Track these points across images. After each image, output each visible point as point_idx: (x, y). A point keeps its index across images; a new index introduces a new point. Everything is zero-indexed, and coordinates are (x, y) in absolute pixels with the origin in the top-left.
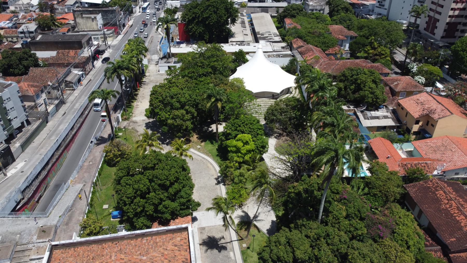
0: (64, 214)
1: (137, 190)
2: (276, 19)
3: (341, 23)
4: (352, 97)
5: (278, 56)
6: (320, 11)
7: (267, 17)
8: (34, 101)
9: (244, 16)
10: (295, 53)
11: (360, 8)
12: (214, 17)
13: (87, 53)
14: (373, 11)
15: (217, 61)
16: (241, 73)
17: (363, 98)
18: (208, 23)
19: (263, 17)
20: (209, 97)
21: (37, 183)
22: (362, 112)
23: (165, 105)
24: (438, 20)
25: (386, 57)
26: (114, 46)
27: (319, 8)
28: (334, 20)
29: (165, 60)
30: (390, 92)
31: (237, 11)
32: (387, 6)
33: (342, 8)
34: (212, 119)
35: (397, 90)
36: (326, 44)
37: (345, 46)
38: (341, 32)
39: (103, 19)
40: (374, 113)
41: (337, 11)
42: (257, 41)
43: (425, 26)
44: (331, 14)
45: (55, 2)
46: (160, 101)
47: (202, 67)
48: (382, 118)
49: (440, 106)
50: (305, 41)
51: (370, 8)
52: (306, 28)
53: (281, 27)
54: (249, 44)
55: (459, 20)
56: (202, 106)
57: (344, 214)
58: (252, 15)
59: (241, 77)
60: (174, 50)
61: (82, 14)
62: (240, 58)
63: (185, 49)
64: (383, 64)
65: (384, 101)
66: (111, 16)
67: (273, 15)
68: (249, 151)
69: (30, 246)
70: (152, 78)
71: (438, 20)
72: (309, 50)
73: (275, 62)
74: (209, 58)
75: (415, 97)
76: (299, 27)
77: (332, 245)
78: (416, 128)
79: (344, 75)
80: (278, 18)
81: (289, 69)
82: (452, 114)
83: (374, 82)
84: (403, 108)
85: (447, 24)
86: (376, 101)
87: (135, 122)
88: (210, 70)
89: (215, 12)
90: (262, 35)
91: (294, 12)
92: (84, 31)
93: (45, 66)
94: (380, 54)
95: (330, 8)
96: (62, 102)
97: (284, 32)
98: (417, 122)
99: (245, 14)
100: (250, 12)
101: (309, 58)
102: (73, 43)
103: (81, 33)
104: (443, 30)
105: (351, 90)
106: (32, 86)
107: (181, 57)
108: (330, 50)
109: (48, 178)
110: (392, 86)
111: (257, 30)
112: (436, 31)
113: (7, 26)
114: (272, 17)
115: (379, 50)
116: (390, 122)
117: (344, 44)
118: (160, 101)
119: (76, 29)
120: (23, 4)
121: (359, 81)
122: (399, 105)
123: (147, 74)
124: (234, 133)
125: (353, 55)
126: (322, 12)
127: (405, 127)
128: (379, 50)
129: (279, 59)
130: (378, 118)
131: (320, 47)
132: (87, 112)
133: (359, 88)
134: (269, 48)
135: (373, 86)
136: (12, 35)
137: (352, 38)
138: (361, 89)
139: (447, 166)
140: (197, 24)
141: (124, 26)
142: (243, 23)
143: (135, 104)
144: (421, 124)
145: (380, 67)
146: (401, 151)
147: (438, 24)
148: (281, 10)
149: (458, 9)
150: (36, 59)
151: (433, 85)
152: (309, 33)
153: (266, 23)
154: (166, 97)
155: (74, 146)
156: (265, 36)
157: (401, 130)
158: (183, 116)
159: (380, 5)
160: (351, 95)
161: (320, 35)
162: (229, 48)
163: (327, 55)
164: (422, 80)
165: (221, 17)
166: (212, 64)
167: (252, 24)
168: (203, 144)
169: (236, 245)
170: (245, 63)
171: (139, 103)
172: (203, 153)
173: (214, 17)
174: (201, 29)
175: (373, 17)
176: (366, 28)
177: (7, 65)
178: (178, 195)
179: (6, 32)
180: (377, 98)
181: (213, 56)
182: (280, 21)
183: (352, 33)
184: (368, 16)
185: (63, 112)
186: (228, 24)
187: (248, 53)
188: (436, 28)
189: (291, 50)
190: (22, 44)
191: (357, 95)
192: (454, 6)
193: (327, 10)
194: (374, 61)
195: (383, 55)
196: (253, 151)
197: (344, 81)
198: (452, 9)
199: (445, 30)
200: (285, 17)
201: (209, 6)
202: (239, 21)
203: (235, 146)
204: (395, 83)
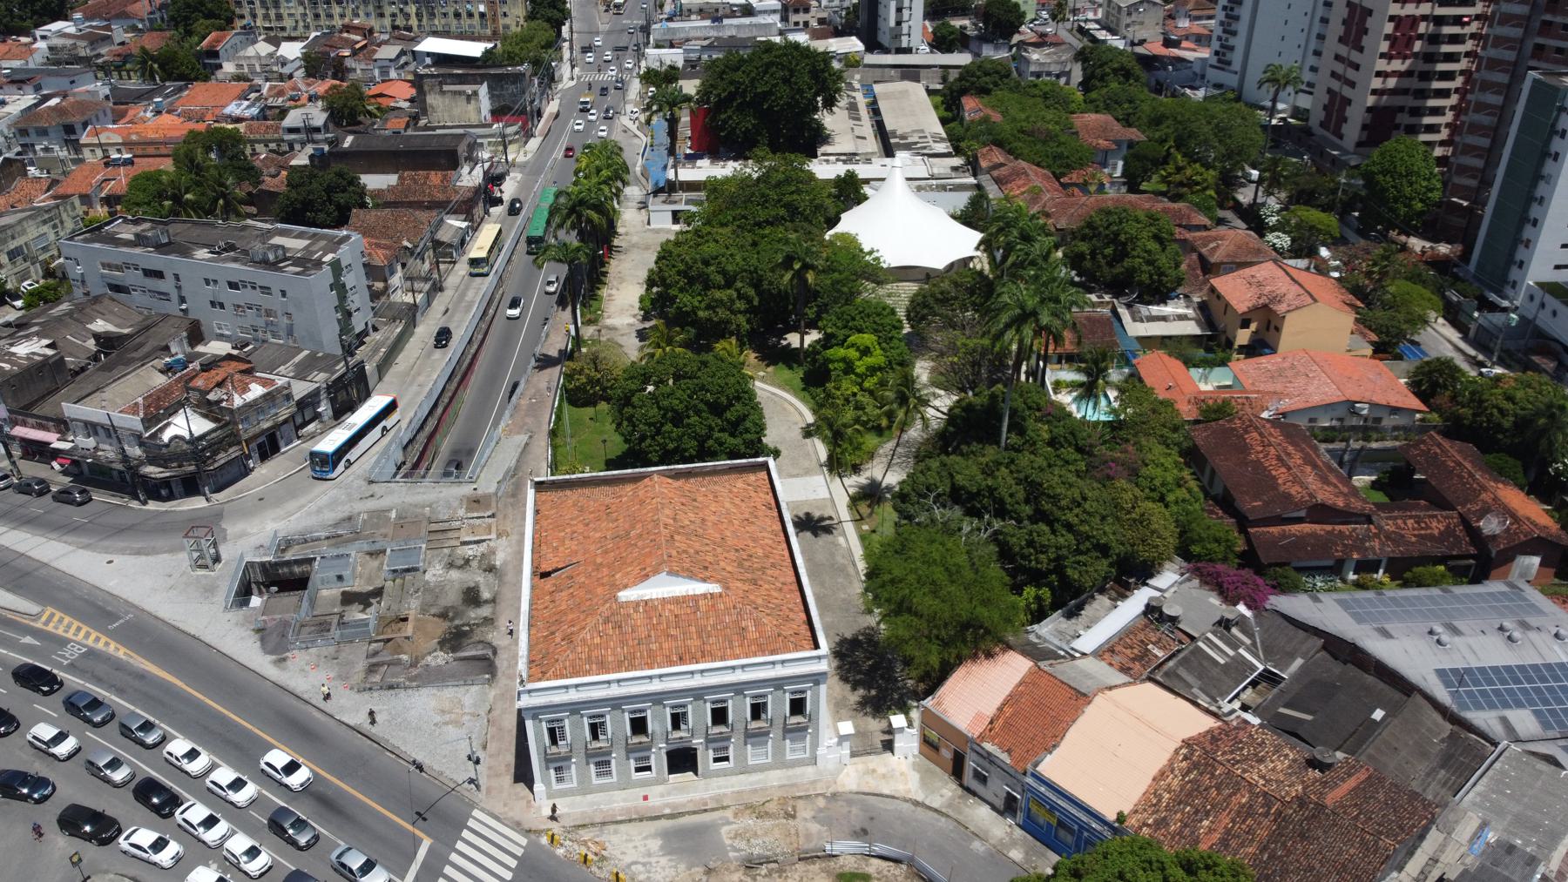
0: (504, 478)
1: (666, 410)
2: (939, 99)
3: (1108, 108)
4: (1107, 272)
5: (943, 188)
6: (1058, 76)
7: (916, 92)
8: (385, 281)
9: (854, 90)
10: (985, 180)
11: (1166, 69)
12: (784, 91)
13: (470, 177)
14: (1203, 77)
15: (798, 192)
16: (851, 223)
17: (1131, 272)
18: (762, 105)
19: (905, 93)
20: (788, 262)
21: (422, 437)
22: (1129, 306)
23: (691, 281)
24: (1349, 102)
25: (1205, 189)
26: (523, 166)
27: (1055, 69)
28: (1092, 101)
29: (662, 197)
30: (1198, 265)
31: (839, 76)
32: (1236, 66)
33: (1115, 71)
34: (786, 322)
35: (1212, 260)
36: (1063, 161)
37: (1114, 168)
38: (1103, 131)
39: (492, 97)
40: (1155, 310)
41: (1102, 79)
42: (889, 151)
43: (1322, 115)
44: (1086, 85)
45: (346, 53)
46: (679, 273)
47: (763, 204)
48: (1176, 318)
49: (1295, 289)
50: (1010, 152)
51: (1197, 69)
52: (1014, 120)
53: (953, 120)
54: (868, 161)
55: (1399, 101)
56: (771, 283)
57: (1046, 436)
58: (877, 88)
59: (853, 232)
60: (687, 174)
61: (441, 83)
62: (850, 192)
63: (704, 170)
64: (1196, 205)
65: (1179, 281)
66: (512, 88)
67: (932, 87)
68: (872, 370)
69: (456, 524)
70: (635, 239)
71: (1349, 102)
72: (1018, 173)
73: (934, 202)
74: (779, 184)
75: (1247, 272)
76: (996, 117)
77: (1019, 472)
78: (1243, 337)
79: (1090, 225)
80: (944, 95)
81: (967, 218)
82: (1315, 301)
83: (1157, 238)
84: (1219, 297)
85: (1369, 110)
86: (1160, 281)
87: (613, 329)
88: (782, 212)
89: (786, 81)
90: (903, 137)
91: (987, 79)
92: (444, 127)
93: (376, 206)
94: (1190, 184)
95: (1084, 69)
96: (437, 288)
97: (959, 130)
98: (1245, 324)
99: (857, 85)
100: (870, 81)
101: (1017, 189)
102: (437, 153)
103: (439, 132)
104: (1359, 127)
105: (1105, 257)
106: (378, 246)
107: (711, 186)
108: (1074, 176)
109: (438, 436)
110: (1204, 251)
111: (889, 127)
112: (1345, 129)
113: (247, 114)
114: (930, 92)
115: (1189, 172)
116: (1191, 328)
117: (1111, 162)
118: (679, 273)
119: (422, 122)
120: (259, 58)
121: (1123, 237)
122: (1213, 290)
123: (620, 230)
124: (841, 334)
125: (1132, 182)
126: (1063, 80)
127: (1223, 338)
128: (1189, 172)
129: (943, 194)
130: (1164, 319)
131: (1048, 167)
132: (491, 311)
133: (1122, 253)
134: (920, 169)
135: (1153, 246)
136: (268, 137)
137: (1131, 144)
138: (1127, 255)
139: (1286, 404)
140: (741, 108)
141: (540, 114)
142: (853, 107)
143: (604, 292)
144: (1253, 326)
145: (1185, 211)
146: (1209, 382)
147: (1349, 112)
148: (953, 75)
149: (1394, 73)
150: (362, 192)
151: (1311, 253)
152: (1023, 132)
153: (912, 108)
154: (695, 262)
155: (475, 379)
156: (910, 140)
157: (1212, 345)
158: (732, 301)
159: (1219, 61)
160: (1106, 269)
161: (1050, 137)
162: (824, 169)
163: (1064, 186)
164: (1283, 241)
165: (801, 92)
166: (788, 198)
167: (875, 111)
168: (770, 369)
169: (850, 528)
170: (859, 203)
171: (614, 292)
172: (772, 384)
173: (784, 91)
174: (750, 122)
175: (1201, 94)
176: (1169, 122)
177: (302, 203)
178: (741, 428)
179: (249, 128)
180: (1162, 274)
181: (788, 181)
182: (949, 102)
183: (1134, 134)
184: (1188, 91)
185: (443, 309)
186: (816, 110)
187: (867, 181)
188: (1345, 120)
189: (975, 175)
190: (311, 157)
191: (1118, 269)
192: (1382, 65)
193: (1077, 74)
194: (1176, 198)
195: (1197, 184)
196: (880, 369)
197: (1091, 239)
198: (1379, 74)
199: (1364, 127)
200: (964, 92)
201: (769, 65)
202: (843, 102)
203: (843, 360)
204: (1212, 245)
